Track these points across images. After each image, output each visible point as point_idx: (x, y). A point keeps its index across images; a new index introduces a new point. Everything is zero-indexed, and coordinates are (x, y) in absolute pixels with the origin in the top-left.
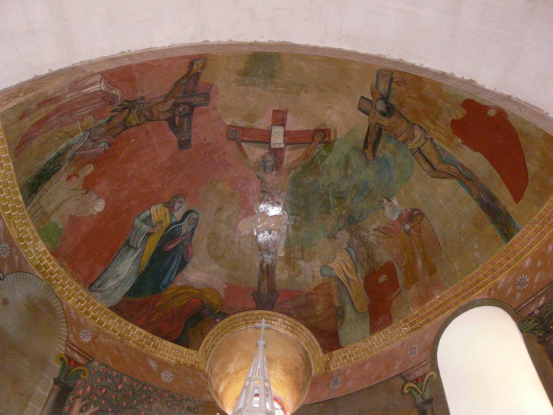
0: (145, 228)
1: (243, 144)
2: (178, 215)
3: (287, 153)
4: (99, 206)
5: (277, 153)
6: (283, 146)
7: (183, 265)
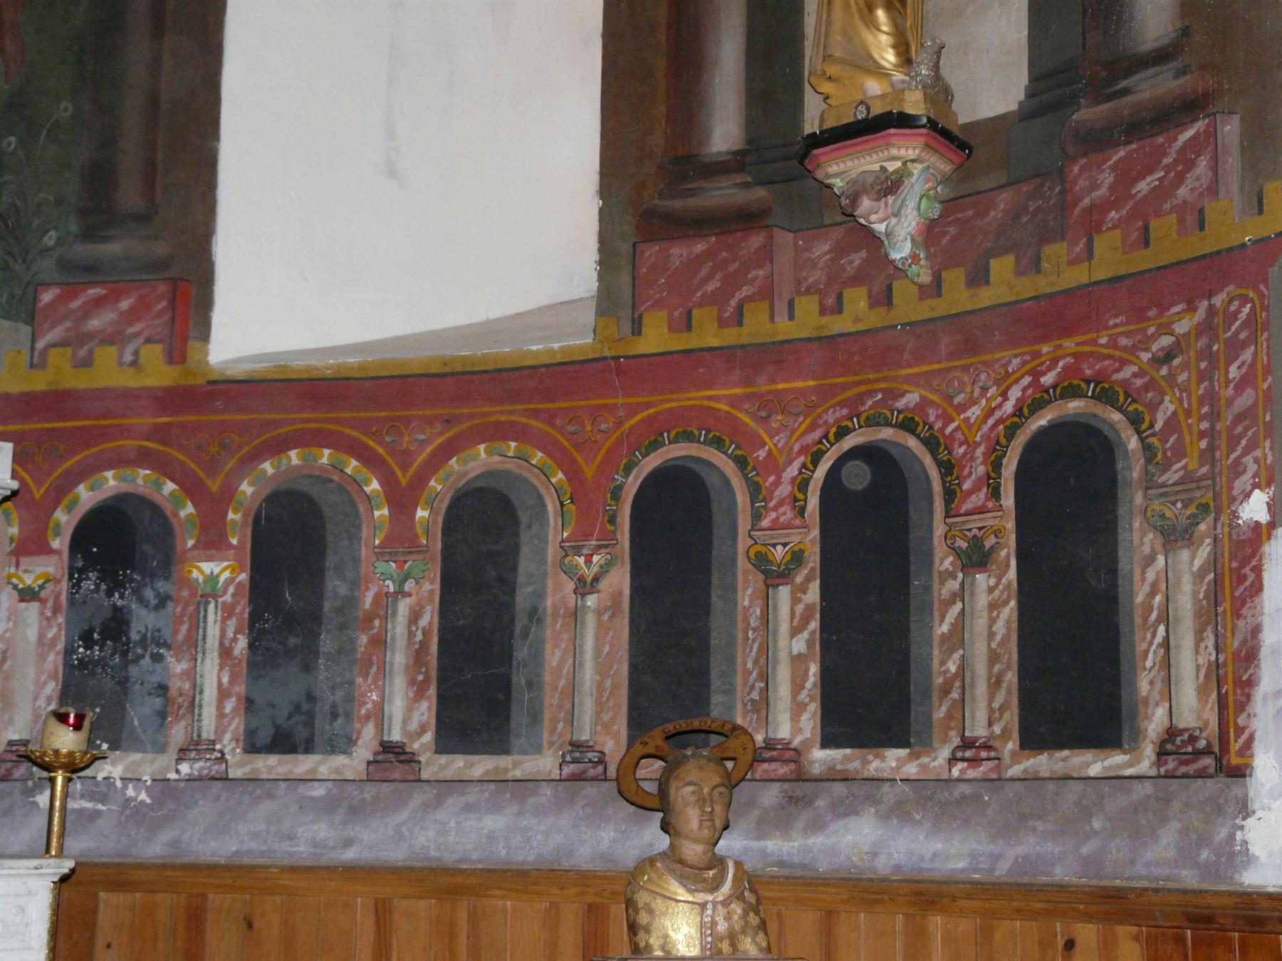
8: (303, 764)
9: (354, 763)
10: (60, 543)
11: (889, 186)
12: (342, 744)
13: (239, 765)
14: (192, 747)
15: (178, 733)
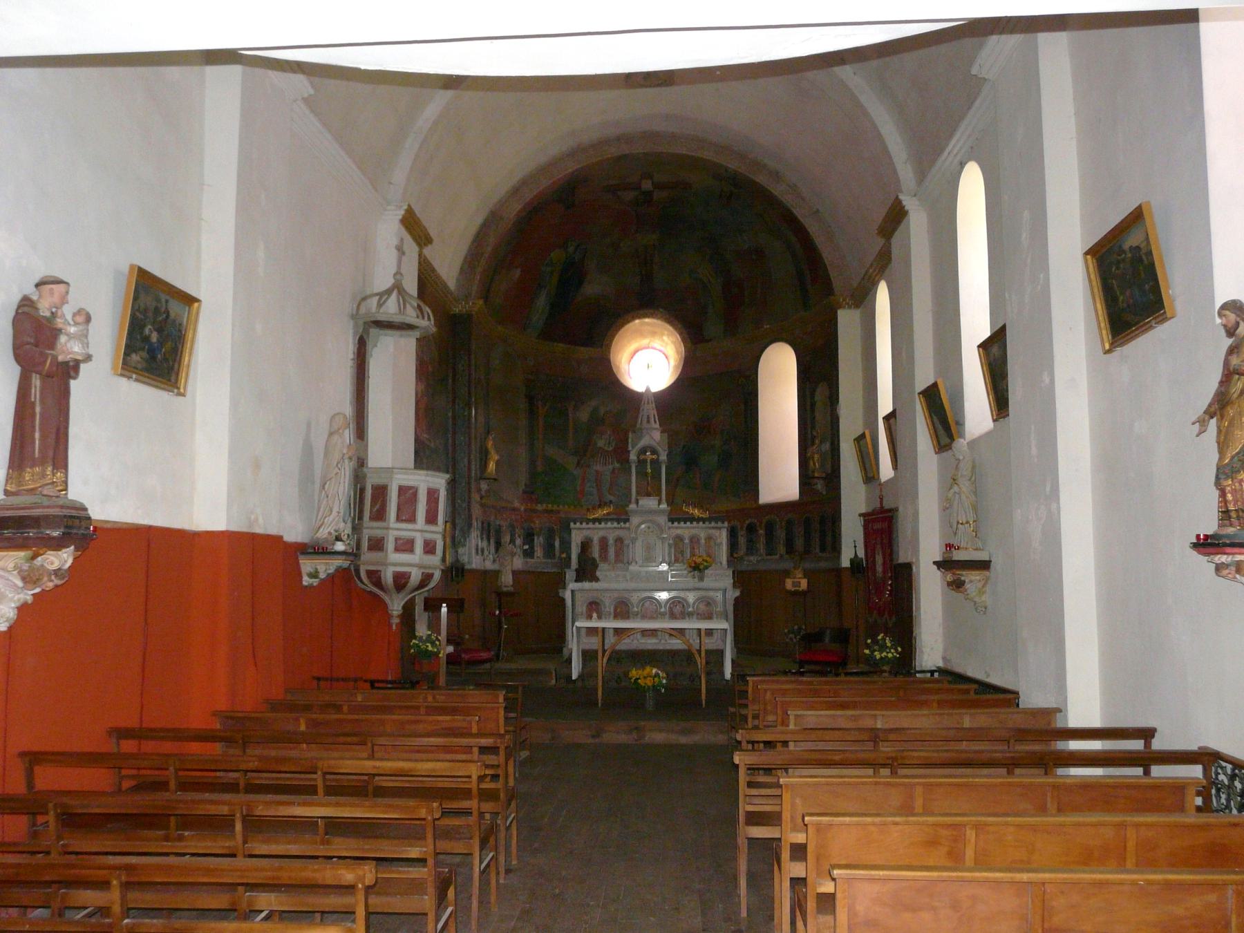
0: (549, 269)
1: (619, 193)
2: (571, 249)
3: (655, 193)
4: (517, 273)
5: (649, 194)
6: (652, 189)
7: (581, 283)
8: (772, 557)
9: (777, 557)
10: (745, 529)
11: (817, 484)
12: (776, 555)
13: (765, 557)
14: (761, 555)
15: (759, 553)
